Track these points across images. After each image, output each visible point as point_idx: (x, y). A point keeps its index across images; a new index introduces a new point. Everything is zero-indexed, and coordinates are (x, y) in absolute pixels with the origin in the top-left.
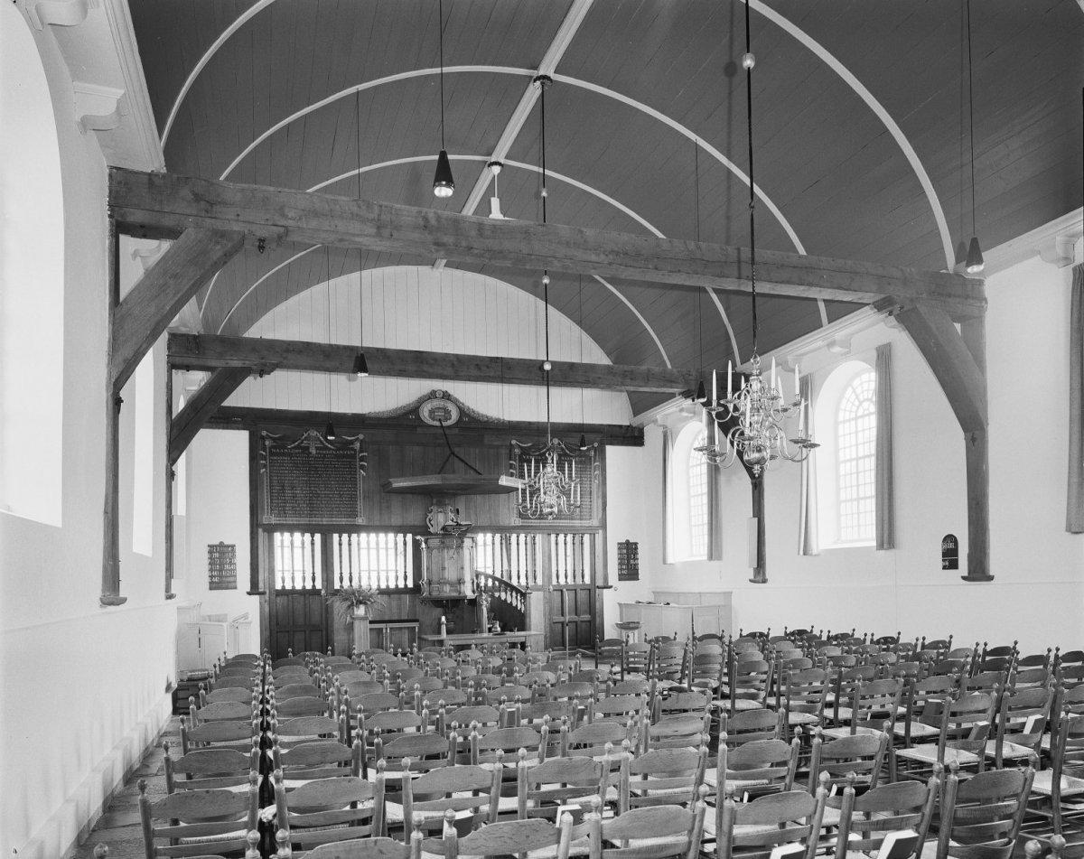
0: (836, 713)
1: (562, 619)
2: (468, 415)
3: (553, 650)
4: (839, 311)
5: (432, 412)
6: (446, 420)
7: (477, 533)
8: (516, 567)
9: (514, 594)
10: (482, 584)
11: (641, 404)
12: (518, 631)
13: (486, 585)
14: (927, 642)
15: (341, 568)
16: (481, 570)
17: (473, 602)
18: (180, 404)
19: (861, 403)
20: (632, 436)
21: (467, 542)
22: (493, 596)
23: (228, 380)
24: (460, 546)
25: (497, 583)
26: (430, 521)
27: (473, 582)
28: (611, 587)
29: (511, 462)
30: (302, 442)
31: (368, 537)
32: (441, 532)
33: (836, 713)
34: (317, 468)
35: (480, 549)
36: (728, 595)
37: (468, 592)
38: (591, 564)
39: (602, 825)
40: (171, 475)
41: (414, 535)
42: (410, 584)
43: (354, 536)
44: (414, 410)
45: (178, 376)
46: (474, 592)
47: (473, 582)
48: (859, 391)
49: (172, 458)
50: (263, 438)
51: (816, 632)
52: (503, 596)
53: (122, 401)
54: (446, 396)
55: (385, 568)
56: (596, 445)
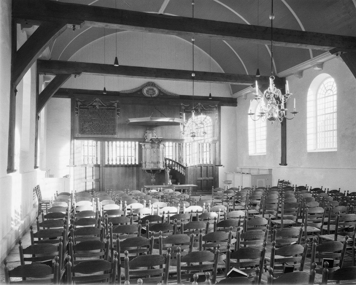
0: (328, 227)
1: (201, 179)
2: (163, 93)
3: (202, 196)
4: (316, 53)
5: (147, 91)
6: (154, 94)
7: (165, 142)
8: (127, 153)
9: (181, 168)
10: (167, 164)
11: (236, 89)
12: (180, 184)
13: (169, 164)
14: (349, 193)
15: (112, 155)
16: (167, 157)
17: (163, 172)
18: (42, 88)
19: (327, 91)
20: (232, 102)
21: (161, 146)
22: (171, 169)
23: (60, 79)
24: (158, 147)
25: (174, 163)
26: (146, 137)
27: (163, 163)
28: (222, 166)
29: (180, 112)
30: (93, 104)
31: (128, 143)
32: (151, 141)
33: (328, 227)
34: (99, 114)
35: (167, 148)
36: (270, 170)
37: (161, 167)
38: (37, 148)
39: (213, 267)
40: (38, 118)
41: (140, 142)
42: (137, 163)
43: (110, 142)
44: (140, 90)
45: (41, 77)
46: (164, 167)
47: (163, 163)
48: (326, 86)
49: (38, 109)
50: (77, 101)
51: (342, 191)
52: (176, 168)
53: (17, 91)
54: (153, 84)
55: (132, 157)
56: (216, 106)
